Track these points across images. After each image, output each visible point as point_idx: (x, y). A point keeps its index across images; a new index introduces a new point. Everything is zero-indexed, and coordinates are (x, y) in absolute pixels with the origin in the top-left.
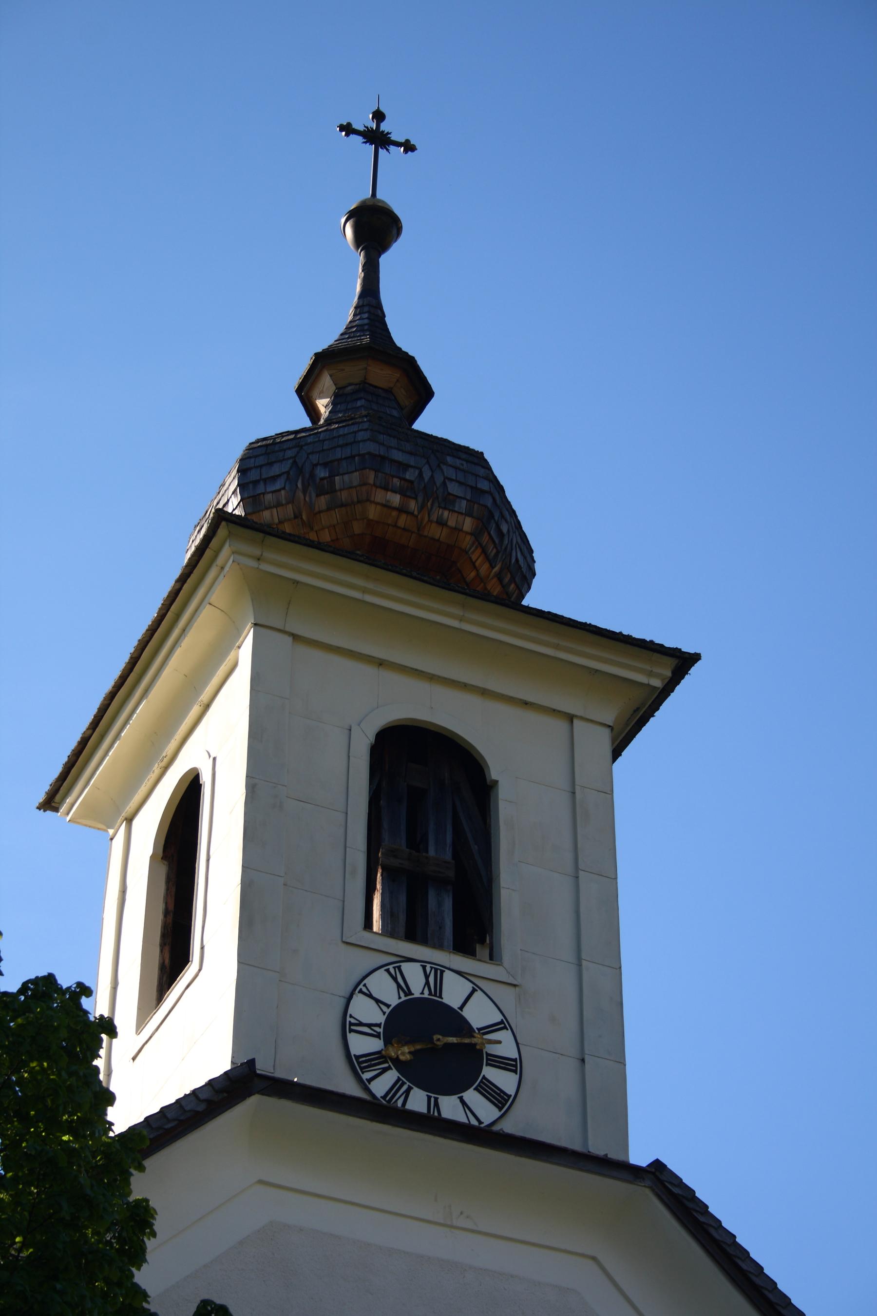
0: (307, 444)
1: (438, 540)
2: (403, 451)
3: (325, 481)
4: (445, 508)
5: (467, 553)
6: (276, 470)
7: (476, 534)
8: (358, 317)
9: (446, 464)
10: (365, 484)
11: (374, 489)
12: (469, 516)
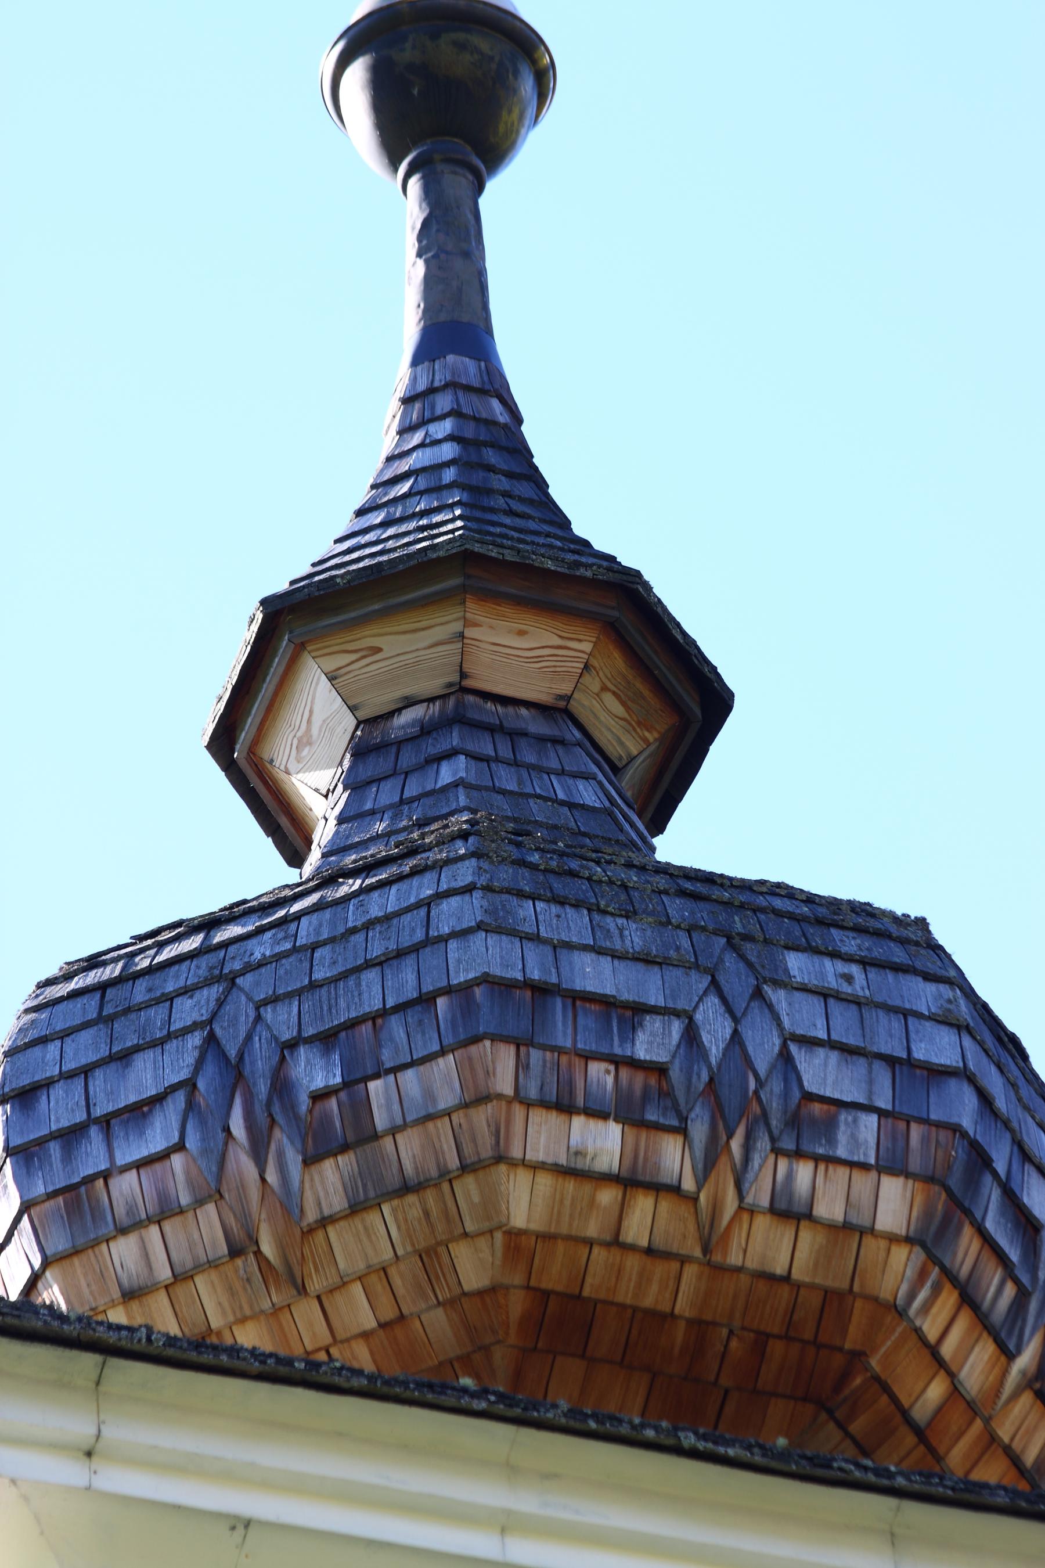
0: (250, 968)
1: (787, 1279)
2: (615, 955)
3: (333, 1103)
4: (798, 1154)
5: (901, 1313)
6: (144, 1077)
7: (929, 1239)
8: (417, 438)
9: (784, 983)
10: (483, 1099)
11: (519, 1111)
12: (893, 1171)
